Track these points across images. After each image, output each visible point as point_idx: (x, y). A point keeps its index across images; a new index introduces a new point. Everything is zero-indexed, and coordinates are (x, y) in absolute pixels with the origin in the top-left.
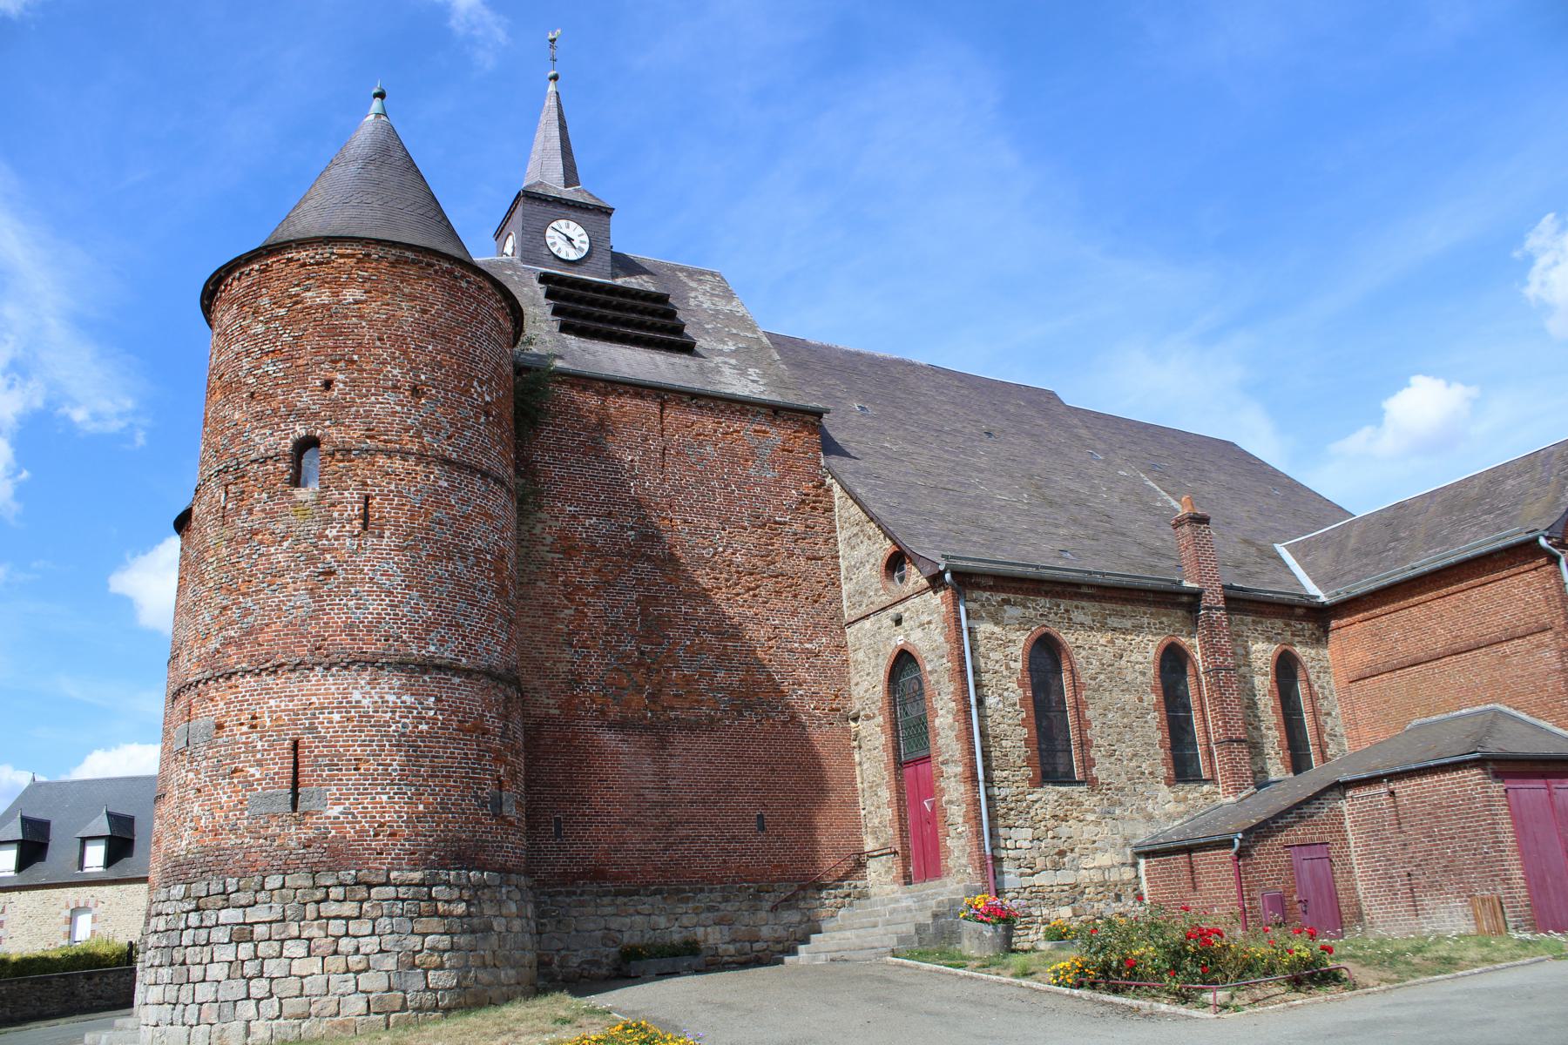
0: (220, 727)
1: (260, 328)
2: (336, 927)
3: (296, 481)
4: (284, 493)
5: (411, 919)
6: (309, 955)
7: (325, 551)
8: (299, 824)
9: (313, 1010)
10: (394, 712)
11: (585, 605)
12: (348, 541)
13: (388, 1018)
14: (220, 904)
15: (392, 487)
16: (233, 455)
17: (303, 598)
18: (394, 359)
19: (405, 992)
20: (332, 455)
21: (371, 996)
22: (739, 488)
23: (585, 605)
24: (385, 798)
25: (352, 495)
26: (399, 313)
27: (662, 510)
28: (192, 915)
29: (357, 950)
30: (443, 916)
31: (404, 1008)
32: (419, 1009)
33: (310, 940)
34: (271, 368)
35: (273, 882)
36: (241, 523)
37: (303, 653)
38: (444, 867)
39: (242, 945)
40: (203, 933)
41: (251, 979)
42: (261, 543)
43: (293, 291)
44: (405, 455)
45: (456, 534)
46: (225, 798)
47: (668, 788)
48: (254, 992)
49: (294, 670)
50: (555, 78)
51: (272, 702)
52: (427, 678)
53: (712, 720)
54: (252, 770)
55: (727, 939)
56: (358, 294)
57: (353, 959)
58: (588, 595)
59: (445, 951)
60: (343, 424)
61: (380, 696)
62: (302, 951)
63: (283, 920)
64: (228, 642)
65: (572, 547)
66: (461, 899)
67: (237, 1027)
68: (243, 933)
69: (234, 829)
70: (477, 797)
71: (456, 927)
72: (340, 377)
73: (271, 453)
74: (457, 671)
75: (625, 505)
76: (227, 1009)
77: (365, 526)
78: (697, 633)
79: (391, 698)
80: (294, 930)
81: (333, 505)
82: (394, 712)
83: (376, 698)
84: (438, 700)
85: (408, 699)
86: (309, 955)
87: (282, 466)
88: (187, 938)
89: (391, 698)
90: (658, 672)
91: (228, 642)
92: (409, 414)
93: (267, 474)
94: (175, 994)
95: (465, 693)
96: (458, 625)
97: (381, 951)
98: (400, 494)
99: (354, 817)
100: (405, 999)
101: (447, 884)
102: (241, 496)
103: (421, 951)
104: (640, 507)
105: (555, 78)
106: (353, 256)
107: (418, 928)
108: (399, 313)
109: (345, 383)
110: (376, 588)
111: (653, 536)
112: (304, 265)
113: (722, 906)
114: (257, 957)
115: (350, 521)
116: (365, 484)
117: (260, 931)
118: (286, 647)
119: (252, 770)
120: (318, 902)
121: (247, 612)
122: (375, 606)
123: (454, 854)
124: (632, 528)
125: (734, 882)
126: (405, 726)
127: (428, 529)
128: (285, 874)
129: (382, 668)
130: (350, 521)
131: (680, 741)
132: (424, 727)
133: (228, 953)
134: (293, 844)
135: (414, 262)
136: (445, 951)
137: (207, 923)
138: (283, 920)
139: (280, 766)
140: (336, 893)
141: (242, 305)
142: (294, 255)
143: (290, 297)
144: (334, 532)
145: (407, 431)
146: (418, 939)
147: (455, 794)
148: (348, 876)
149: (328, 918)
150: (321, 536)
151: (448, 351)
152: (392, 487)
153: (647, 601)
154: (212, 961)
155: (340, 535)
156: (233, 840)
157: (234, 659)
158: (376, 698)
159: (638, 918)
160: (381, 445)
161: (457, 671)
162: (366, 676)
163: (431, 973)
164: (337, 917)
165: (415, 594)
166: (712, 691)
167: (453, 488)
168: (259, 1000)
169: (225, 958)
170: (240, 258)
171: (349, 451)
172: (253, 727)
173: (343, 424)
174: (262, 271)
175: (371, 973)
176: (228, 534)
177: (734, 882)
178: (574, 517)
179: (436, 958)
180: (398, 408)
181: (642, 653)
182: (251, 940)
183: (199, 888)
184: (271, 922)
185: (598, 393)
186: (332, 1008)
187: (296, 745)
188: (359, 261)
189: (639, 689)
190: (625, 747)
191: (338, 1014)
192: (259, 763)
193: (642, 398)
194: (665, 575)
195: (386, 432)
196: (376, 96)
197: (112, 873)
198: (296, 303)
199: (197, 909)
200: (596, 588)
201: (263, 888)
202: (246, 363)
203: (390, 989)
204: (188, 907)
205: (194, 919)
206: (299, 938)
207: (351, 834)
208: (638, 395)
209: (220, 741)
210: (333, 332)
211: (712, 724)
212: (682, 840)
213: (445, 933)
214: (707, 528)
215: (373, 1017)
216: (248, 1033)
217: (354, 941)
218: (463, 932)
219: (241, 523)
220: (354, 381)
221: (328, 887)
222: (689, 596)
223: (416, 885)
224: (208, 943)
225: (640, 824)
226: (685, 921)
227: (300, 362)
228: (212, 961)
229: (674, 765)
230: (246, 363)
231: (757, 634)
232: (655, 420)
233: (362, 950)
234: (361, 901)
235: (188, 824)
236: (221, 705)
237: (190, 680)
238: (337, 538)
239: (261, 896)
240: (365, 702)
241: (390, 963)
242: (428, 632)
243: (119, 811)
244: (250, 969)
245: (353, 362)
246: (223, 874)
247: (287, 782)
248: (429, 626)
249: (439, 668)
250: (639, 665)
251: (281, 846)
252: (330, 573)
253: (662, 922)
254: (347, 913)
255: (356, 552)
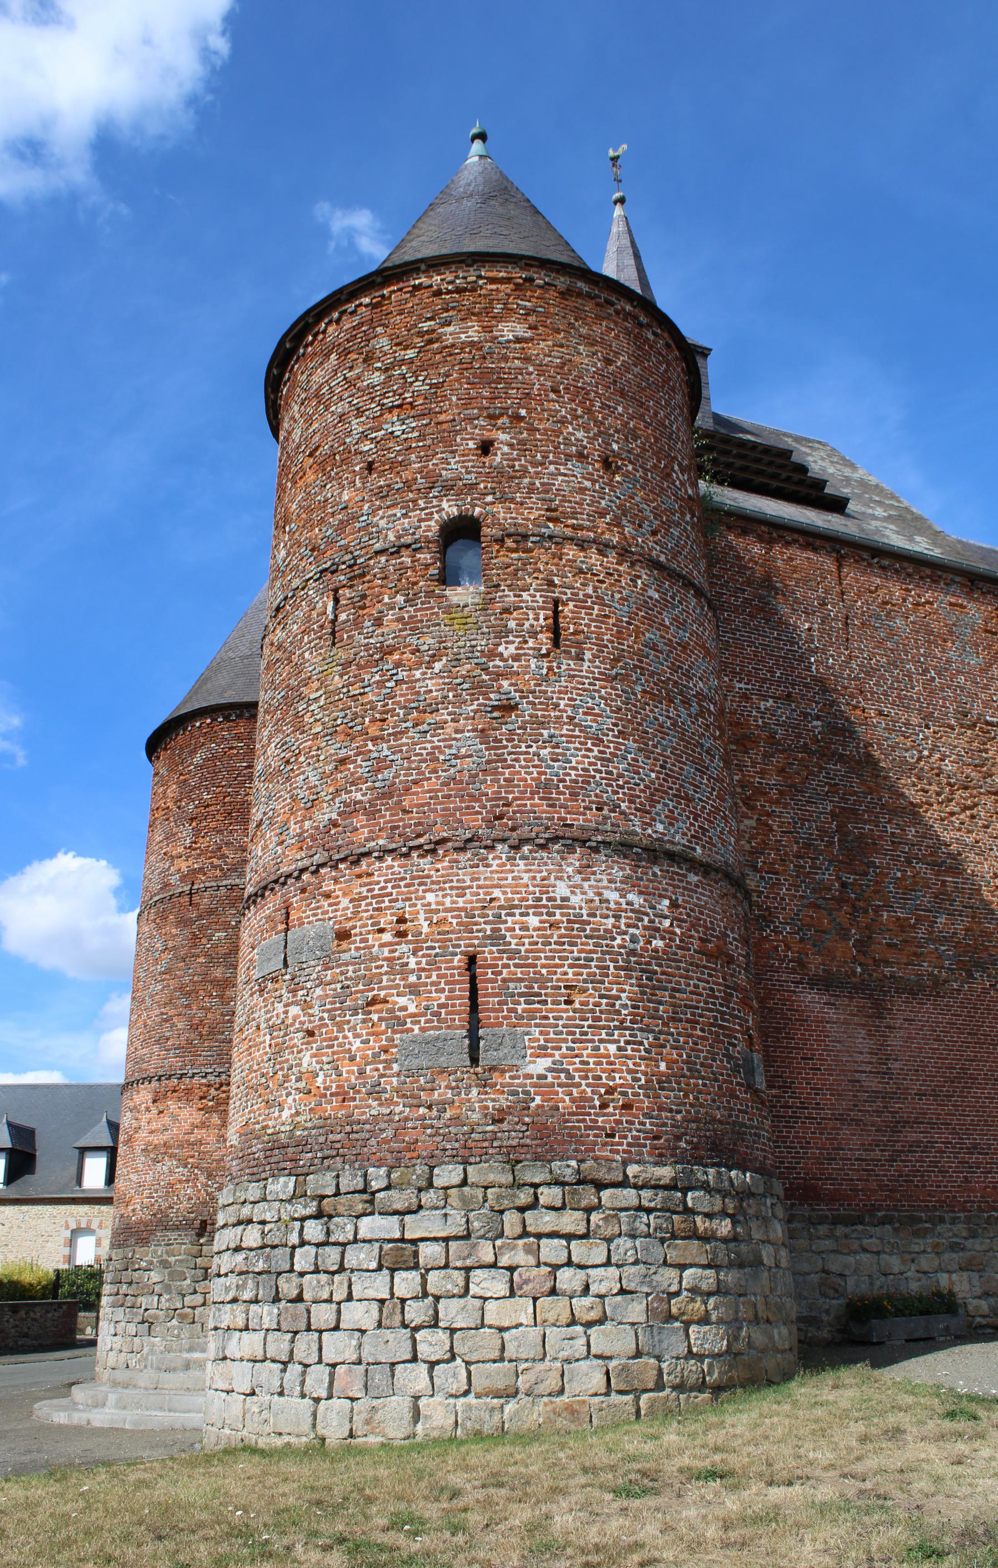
0: (343, 935)
1: (377, 378)
2: (552, 1250)
3: (447, 577)
4: (430, 594)
5: (662, 1241)
6: (512, 1294)
7: (499, 675)
8: (484, 1084)
9: (522, 1383)
10: (617, 917)
11: (768, 815)
12: (533, 662)
13: (637, 1399)
14: (360, 1207)
15: (590, 590)
16: (346, 549)
17: (469, 742)
18: (576, 417)
19: (659, 1358)
20: (501, 541)
21: (612, 1364)
22: (939, 674)
23: (768, 815)
24: (612, 1048)
25: (534, 597)
26: (577, 359)
27: (852, 696)
28: (308, 1223)
29: (586, 1290)
30: (705, 1238)
31: (659, 1386)
32: (680, 1388)
33: (511, 1269)
34: (398, 429)
35: (448, 1175)
36: (364, 639)
37: (476, 823)
38: (699, 1161)
39: (399, 1276)
40: (332, 1254)
41: (416, 1329)
42: (398, 665)
43: (425, 326)
44: (603, 548)
45: (675, 668)
46: (357, 1044)
47: (888, 1072)
48: (423, 1350)
49: (462, 849)
50: (622, 201)
51: (430, 897)
52: (656, 869)
53: (936, 982)
54: (402, 1001)
55: (978, 1291)
56: (521, 330)
57: (581, 1303)
58: (771, 802)
59: (710, 1294)
60: (512, 500)
61: (593, 890)
62: (503, 1289)
63: (467, 1237)
64: (351, 810)
65: (745, 737)
66: (724, 1214)
67: (399, 1405)
68: (400, 1256)
69: (375, 1092)
70: (729, 1057)
71: (722, 1258)
72: (503, 437)
73: (408, 539)
74: (695, 865)
75: (806, 685)
76: (379, 1376)
77: (556, 643)
78: (909, 862)
79: (613, 896)
80: (486, 1252)
81: (506, 611)
82: (617, 917)
83: (591, 895)
84: (674, 905)
85: (636, 899)
86: (512, 1294)
87: (425, 557)
88: (303, 1259)
89: (613, 896)
90: (866, 912)
91: (351, 810)
92: (602, 495)
93: (402, 569)
94: (285, 1346)
95: (705, 897)
96: (689, 799)
97: (622, 1291)
98: (600, 600)
99: (569, 1076)
100: (660, 1371)
101: (705, 1187)
102: (360, 604)
103: (677, 1294)
104: (825, 690)
105: (622, 201)
106: (508, 280)
107: (673, 1256)
108: (577, 359)
109: (511, 446)
110: (577, 735)
111: (843, 729)
112: (438, 293)
113: (969, 1243)
114: (425, 1294)
115: (534, 634)
116: (551, 584)
117: (429, 1252)
118: (447, 815)
119: (402, 1001)
120: (522, 1210)
121: (381, 765)
122: (580, 759)
123: (710, 1144)
124: (818, 718)
125: (980, 1210)
126: (634, 939)
127: (641, 655)
128: (466, 1163)
129: (596, 850)
130: (534, 634)
131: (900, 1008)
132: (658, 943)
133: (378, 1286)
134: (475, 1117)
135: (589, 296)
136: (710, 1294)
137: (337, 1236)
138: (467, 1237)
139: (448, 994)
140: (549, 1195)
141: (347, 352)
142: (423, 280)
143: (421, 334)
144: (512, 649)
145: (602, 514)
146: (673, 1273)
147: (704, 1047)
148: (567, 1168)
149: (539, 1236)
150: (493, 654)
151: (641, 417)
152: (590, 590)
153: (845, 815)
154: (350, 1298)
155: (522, 654)
156: (375, 1108)
157: (362, 833)
158: (591, 895)
159: (865, 1257)
160: (569, 532)
161: (695, 865)
162: (574, 860)
163: (693, 1328)
164: (553, 1235)
165: (632, 745)
166: (934, 941)
167: (665, 604)
168: (432, 1365)
169: (371, 1293)
170: (340, 291)
171: (525, 537)
172: (401, 934)
173: (512, 500)
174: (373, 306)
175: (608, 1326)
176: (342, 655)
177: (980, 1210)
178: (745, 697)
179: (698, 1306)
180: (588, 484)
181: (844, 885)
182: (416, 1267)
183: (323, 1182)
184: (446, 1240)
185: (761, 539)
186: (552, 1382)
187: (472, 960)
188: (518, 287)
189: (845, 936)
190: (832, 1014)
191: (561, 1391)
192: (414, 990)
193: (815, 550)
194: (863, 782)
195: (574, 515)
196: (474, 138)
197: (13, 1193)
198: (430, 342)
199: (318, 1215)
200: (781, 793)
201: (430, 1185)
202: (356, 426)
203: (638, 1354)
204: (301, 1211)
205: (314, 1230)
206: (494, 1265)
207: (566, 1103)
208: (807, 546)
209: (345, 957)
210: (486, 377)
211: (936, 988)
212: (912, 1147)
213: (708, 1266)
214: (907, 724)
215: (615, 1398)
216: (416, 1415)
217: (581, 1274)
218: (731, 1265)
219: (364, 639)
220: (521, 442)
221: (536, 1186)
222: (894, 812)
223: (665, 1188)
224: (341, 1269)
225: (857, 1122)
226: (925, 1262)
227: (442, 418)
228: (350, 1298)
229: (895, 1041)
230: (356, 426)
231: (980, 867)
232: (831, 580)
233: (594, 1289)
234: (589, 1210)
235: (292, 1083)
236: (345, 902)
237: (284, 869)
238: (516, 658)
239: (429, 1197)
240: (576, 900)
241: (636, 1310)
242: (653, 803)
243: (19, 1121)
244: (416, 1312)
245: (519, 418)
246: (361, 1161)
247: (460, 1020)
248: (655, 794)
249: (672, 857)
250: (841, 901)
251: (456, 1120)
252: (508, 708)
253: (895, 1263)
254: (569, 1229)
255: (545, 679)
